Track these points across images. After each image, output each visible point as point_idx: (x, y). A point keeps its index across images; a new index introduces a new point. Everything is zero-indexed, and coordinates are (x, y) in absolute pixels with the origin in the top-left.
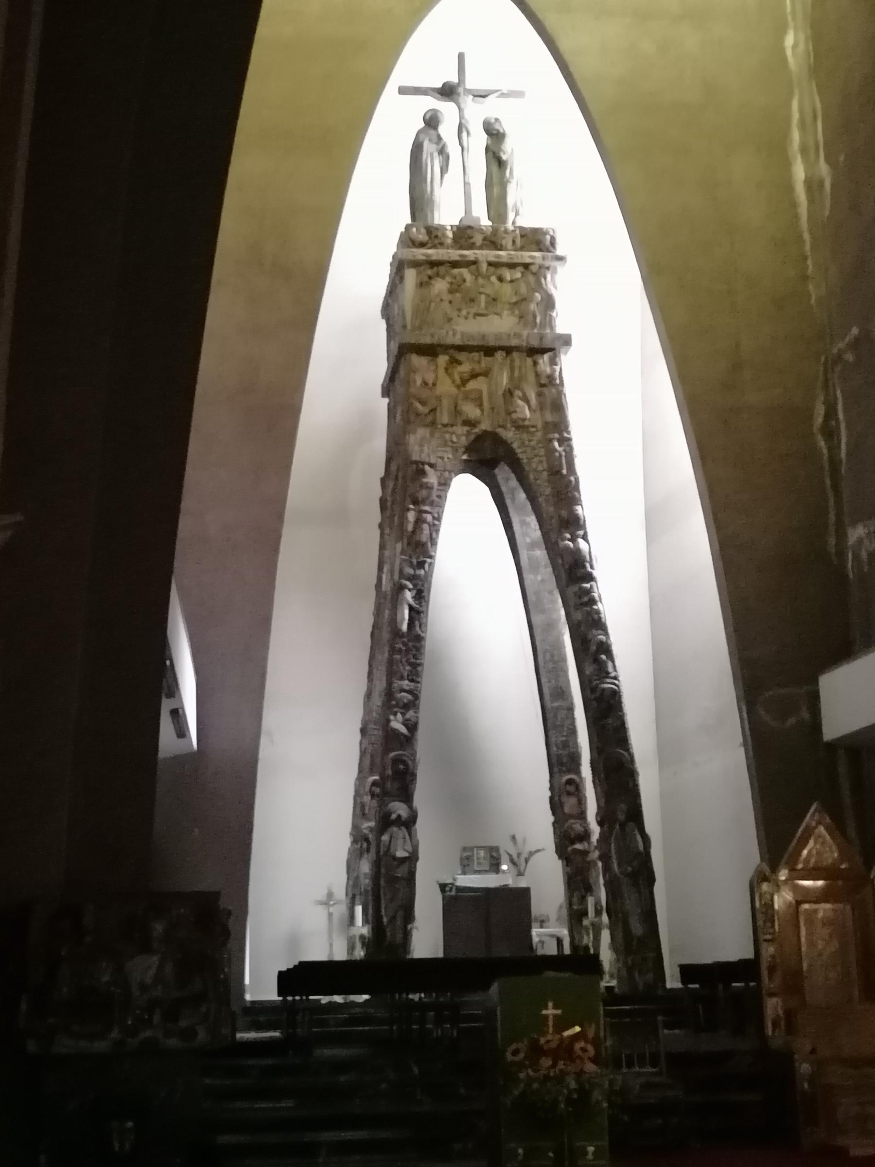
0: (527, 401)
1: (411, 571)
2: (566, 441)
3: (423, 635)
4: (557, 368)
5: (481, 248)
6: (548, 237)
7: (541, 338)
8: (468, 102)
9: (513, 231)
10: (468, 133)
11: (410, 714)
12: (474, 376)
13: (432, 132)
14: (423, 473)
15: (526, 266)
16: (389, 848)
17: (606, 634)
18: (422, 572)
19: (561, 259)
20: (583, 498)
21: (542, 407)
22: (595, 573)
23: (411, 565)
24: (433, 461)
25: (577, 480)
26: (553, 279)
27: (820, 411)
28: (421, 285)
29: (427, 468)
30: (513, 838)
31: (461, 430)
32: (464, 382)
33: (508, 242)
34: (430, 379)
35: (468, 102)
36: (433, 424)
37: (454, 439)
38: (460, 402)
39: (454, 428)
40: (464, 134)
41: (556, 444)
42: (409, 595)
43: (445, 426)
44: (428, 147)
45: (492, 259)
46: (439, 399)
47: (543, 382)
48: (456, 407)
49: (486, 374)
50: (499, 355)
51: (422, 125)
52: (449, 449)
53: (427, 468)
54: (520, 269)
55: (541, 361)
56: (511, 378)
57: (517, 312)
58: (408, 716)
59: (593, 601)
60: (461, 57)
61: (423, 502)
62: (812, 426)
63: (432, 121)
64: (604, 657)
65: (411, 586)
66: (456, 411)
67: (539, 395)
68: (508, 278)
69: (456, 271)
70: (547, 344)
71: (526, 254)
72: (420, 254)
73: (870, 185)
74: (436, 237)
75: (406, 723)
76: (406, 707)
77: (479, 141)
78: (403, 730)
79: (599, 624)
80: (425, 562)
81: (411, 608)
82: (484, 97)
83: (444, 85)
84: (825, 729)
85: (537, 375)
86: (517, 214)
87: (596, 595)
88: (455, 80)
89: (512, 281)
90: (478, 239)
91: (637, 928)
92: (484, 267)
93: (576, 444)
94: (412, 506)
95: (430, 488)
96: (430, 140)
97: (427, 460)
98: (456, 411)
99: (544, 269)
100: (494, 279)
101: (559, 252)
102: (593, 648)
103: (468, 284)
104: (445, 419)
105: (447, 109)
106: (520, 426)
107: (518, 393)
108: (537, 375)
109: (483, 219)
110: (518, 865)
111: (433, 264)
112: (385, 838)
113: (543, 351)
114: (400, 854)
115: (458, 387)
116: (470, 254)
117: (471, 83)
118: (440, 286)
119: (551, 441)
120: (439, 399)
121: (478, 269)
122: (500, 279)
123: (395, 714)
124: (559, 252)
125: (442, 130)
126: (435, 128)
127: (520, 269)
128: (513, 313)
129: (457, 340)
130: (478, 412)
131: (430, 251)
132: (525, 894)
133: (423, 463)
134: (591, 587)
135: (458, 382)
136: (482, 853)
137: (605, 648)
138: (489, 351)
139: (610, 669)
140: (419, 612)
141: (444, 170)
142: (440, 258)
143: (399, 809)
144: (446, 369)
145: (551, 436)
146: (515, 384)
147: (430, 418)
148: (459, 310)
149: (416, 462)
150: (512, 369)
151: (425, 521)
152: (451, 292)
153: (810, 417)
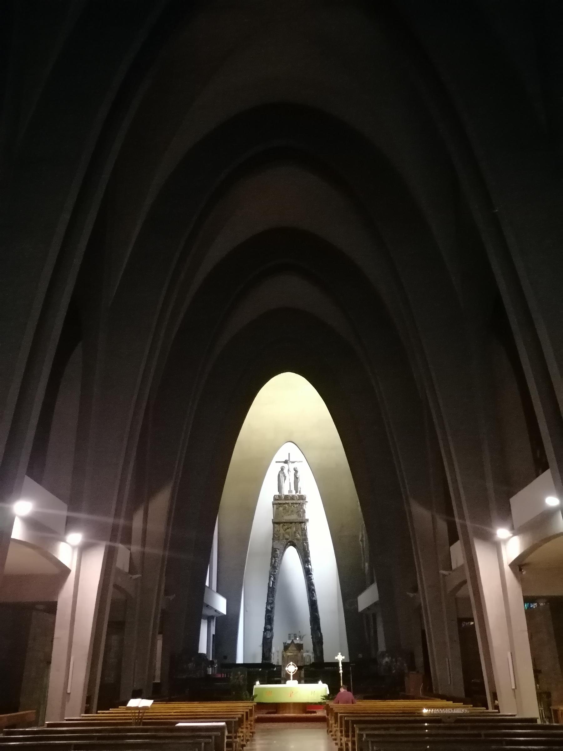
0: (299, 533)
1: (273, 573)
2: (307, 543)
3: (275, 587)
4: (306, 526)
5: (290, 500)
6: (304, 497)
7: (302, 519)
8: (290, 464)
9: (297, 496)
10: (290, 472)
11: (272, 605)
13: (282, 471)
14: (277, 551)
15: (299, 504)
16: (266, 636)
17: (314, 587)
18: (275, 573)
19: (307, 502)
20: (310, 556)
21: (302, 535)
24: (278, 548)
25: (309, 552)
27: (360, 536)
28: (277, 508)
29: (277, 549)
30: (299, 632)
31: (285, 541)
32: (286, 530)
33: (295, 499)
34: (278, 530)
35: (290, 464)
36: (279, 540)
37: (283, 543)
38: (285, 535)
39: (284, 540)
40: (289, 472)
41: (305, 544)
42: (272, 579)
43: (282, 540)
45: (292, 502)
46: (280, 534)
47: (302, 529)
48: (284, 535)
50: (293, 524)
51: (281, 470)
52: (282, 545)
53: (277, 549)
54: (298, 504)
55: (302, 525)
56: (296, 529)
57: (297, 514)
58: (271, 606)
59: (311, 579)
60: (289, 454)
61: (276, 558)
62: (359, 540)
63: (282, 469)
64: (313, 592)
65: (273, 576)
66: (284, 536)
67: (302, 532)
68: (295, 506)
69: (285, 505)
71: (300, 501)
72: (277, 502)
73: (298, 544)
74: (281, 498)
76: (271, 604)
77: (293, 472)
80: (276, 571)
81: (272, 581)
82: (294, 463)
83: (285, 460)
84: (359, 609)
85: (301, 528)
86: (300, 489)
87: (312, 578)
89: (296, 507)
90: (289, 498)
91: (319, 655)
93: (309, 543)
94: (274, 558)
95: (277, 554)
96: (282, 474)
97: (277, 548)
98: (284, 536)
99: (303, 504)
100: (292, 507)
101: (307, 500)
102: (311, 590)
103: (287, 508)
104: (281, 539)
105: (285, 465)
106: (298, 540)
107: (297, 532)
108: (301, 528)
109: (294, 493)
110: (301, 638)
111: (280, 504)
112: (265, 633)
113: (302, 522)
114: (268, 637)
115: (284, 531)
116: (287, 501)
117: (291, 460)
118: (281, 509)
119: (304, 543)
120: (280, 534)
121: (289, 505)
123: (268, 606)
124: (307, 500)
125: (284, 471)
126: (283, 471)
127: (298, 504)
128: (296, 514)
129: (284, 521)
130: (289, 536)
131: (279, 501)
132: (302, 644)
133: (276, 549)
134: (311, 576)
135: (284, 530)
136: (293, 635)
137: (314, 590)
138: (291, 523)
139: (315, 595)
140: (274, 582)
141: (285, 479)
142: (281, 503)
143: (269, 627)
144: (282, 527)
145: (304, 542)
147: (278, 539)
148: (285, 514)
149: (275, 549)
150: (296, 527)
151: (276, 562)
152: (283, 510)
153: (358, 538)
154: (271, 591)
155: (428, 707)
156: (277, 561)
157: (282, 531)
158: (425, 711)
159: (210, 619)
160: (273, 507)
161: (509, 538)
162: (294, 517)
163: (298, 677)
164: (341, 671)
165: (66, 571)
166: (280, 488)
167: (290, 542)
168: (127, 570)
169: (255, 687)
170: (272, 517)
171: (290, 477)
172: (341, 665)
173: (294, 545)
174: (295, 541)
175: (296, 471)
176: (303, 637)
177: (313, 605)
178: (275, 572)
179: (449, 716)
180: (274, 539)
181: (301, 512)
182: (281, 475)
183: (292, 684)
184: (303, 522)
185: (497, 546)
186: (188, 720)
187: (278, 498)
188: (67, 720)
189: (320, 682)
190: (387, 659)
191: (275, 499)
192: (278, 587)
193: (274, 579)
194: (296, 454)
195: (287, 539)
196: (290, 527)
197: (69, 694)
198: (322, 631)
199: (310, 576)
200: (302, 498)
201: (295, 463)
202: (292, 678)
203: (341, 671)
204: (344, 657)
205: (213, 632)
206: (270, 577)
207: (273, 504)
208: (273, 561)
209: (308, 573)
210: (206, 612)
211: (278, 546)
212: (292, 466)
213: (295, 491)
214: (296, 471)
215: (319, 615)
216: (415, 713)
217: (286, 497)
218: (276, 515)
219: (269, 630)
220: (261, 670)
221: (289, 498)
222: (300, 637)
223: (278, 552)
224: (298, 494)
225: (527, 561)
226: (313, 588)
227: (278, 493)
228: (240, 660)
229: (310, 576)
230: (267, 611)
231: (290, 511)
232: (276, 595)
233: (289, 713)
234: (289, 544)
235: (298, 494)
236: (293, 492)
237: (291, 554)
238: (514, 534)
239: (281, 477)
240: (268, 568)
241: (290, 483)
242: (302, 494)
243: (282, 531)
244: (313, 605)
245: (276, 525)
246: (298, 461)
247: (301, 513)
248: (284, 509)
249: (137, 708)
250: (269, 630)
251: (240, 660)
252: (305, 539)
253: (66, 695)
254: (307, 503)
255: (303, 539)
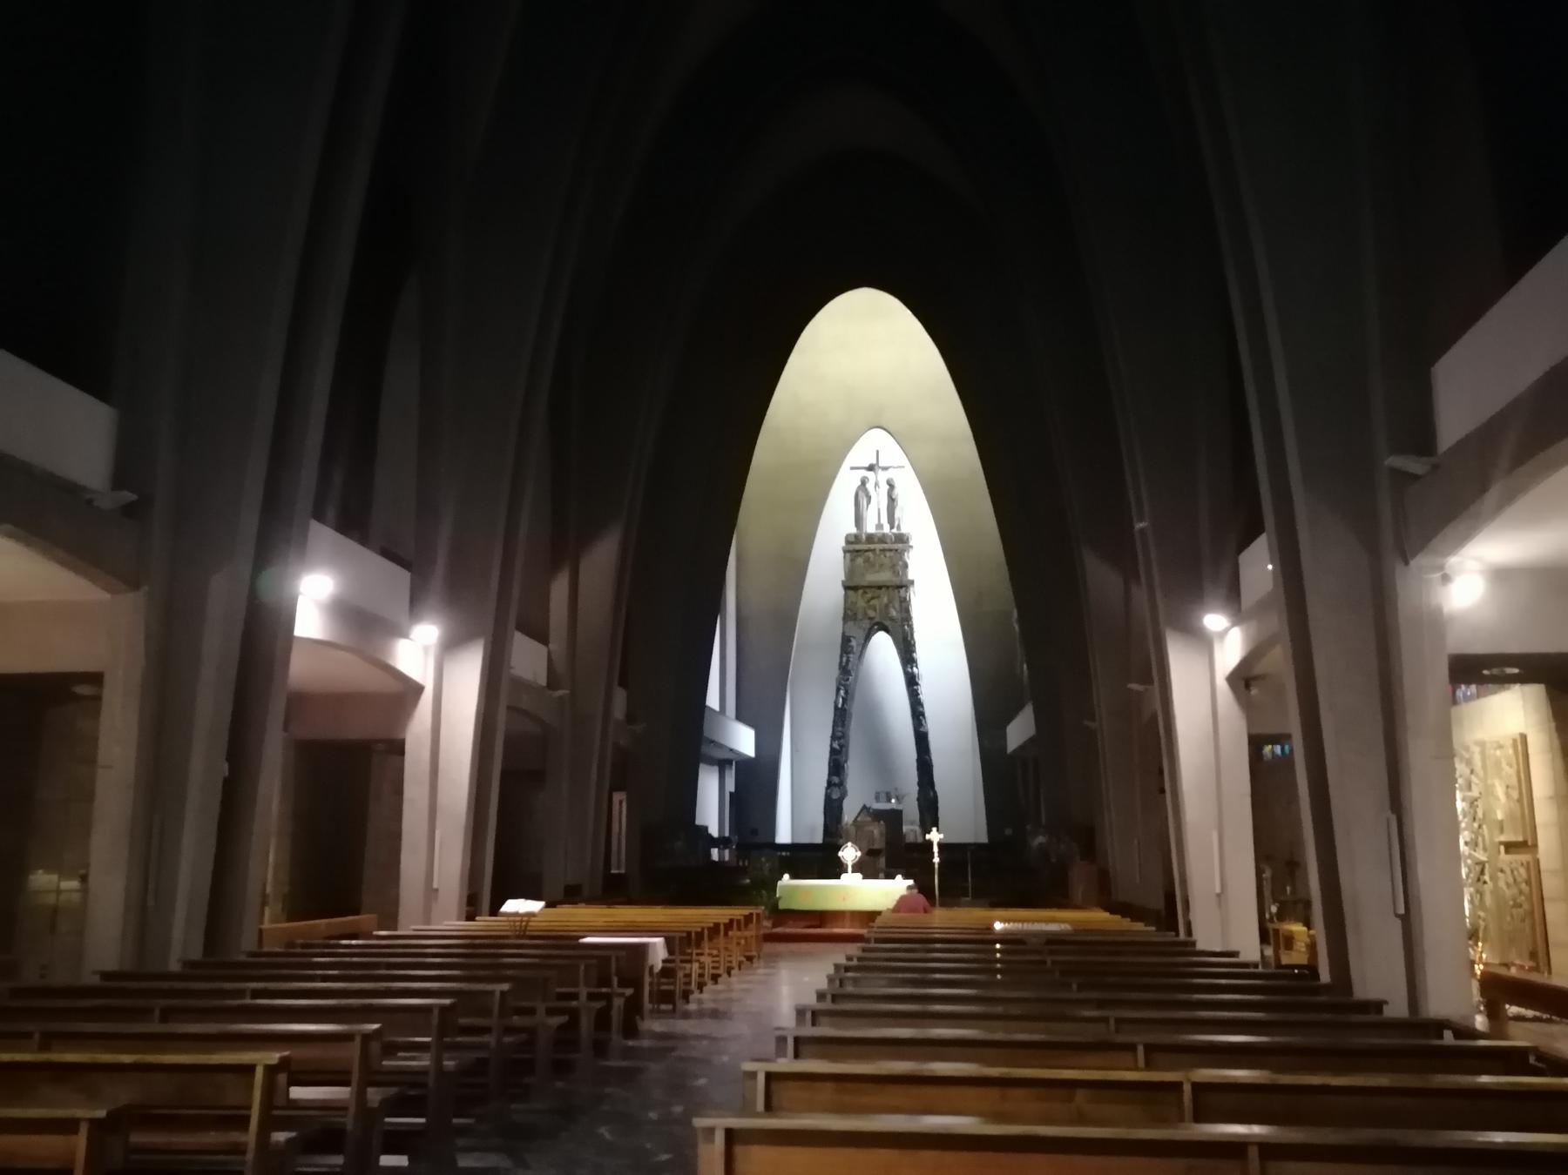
0: (895, 608)
2: (911, 627)
5: (877, 543)
7: (901, 581)
8: (880, 472)
11: (842, 741)
12: (873, 598)
14: (850, 641)
15: (896, 550)
20: (917, 650)
21: (901, 611)
22: (920, 682)
23: (843, 679)
26: (908, 557)
32: (869, 601)
33: (888, 541)
42: (842, 692)
44: (861, 494)
49: (878, 597)
50: (883, 589)
56: (888, 599)
59: (918, 694)
60: (878, 452)
61: (849, 653)
63: (864, 482)
67: (901, 606)
69: (867, 554)
70: (904, 583)
75: (839, 745)
76: (840, 738)
78: (838, 747)
79: (921, 704)
81: (843, 698)
87: (919, 692)
88: (875, 462)
90: (876, 540)
92: (878, 552)
98: (866, 614)
100: (882, 556)
105: (870, 475)
106: (892, 619)
108: (900, 597)
109: (886, 529)
111: (858, 551)
113: (901, 587)
116: (872, 546)
117: (880, 465)
118: (860, 560)
119: (904, 626)
122: (885, 556)
125: (868, 486)
129: (865, 584)
137: (923, 714)
138: (880, 588)
139: (923, 722)
141: (869, 502)
143: (836, 780)
146: (890, 601)
154: (841, 716)
155: (1003, 920)
156: (851, 659)
157: (861, 603)
158: (998, 926)
159: (723, 765)
160: (844, 557)
161: (1226, 631)
162: (884, 577)
163: (859, 867)
164: (936, 860)
165: (417, 689)
166: (859, 520)
167: (877, 624)
168: (543, 681)
169: (779, 883)
170: (843, 577)
171: (879, 499)
172: (936, 849)
173: (887, 631)
174: (887, 623)
175: (891, 486)
176: (903, 798)
177: (922, 740)
178: (848, 679)
179: (1036, 934)
180: (846, 618)
181: (899, 566)
182: (862, 495)
183: (851, 880)
184: (905, 585)
185: (1205, 643)
186: (621, 934)
187: (853, 539)
188: (415, 930)
189: (899, 877)
190: (1041, 839)
191: (848, 542)
192: (855, 709)
193: (846, 693)
194: (892, 453)
195: (871, 619)
196: (876, 595)
197: (437, 890)
198: (937, 788)
199: (915, 687)
200: (902, 539)
201: (890, 470)
202: (850, 869)
203: (936, 860)
204: (942, 836)
205: (730, 786)
206: (838, 690)
207: (845, 551)
208: (844, 659)
209: (912, 682)
210: (705, 749)
211: (857, 633)
212: (883, 477)
213: (889, 526)
214: (891, 486)
215: (931, 760)
216: (1312, 937)
217: (870, 538)
218: (850, 572)
219: (835, 785)
220: (709, 855)
221: (876, 540)
222: (898, 799)
223: (854, 643)
224: (895, 531)
225: (1259, 669)
226: (921, 709)
227: (854, 530)
228: (784, 835)
229: (915, 687)
230: (833, 752)
231: (877, 565)
232: (852, 723)
233: (843, 927)
234: (876, 627)
235: (895, 531)
236: (885, 528)
237: (882, 647)
238: (1234, 624)
239: (860, 499)
240: (835, 672)
241: (879, 510)
242: (904, 530)
243: (861, 603)
244: (922, 740)
245: (851, 593)
246: (895, 466)
247: (899, 568)
248: (867, 560)
249: (516, 914)
250: (835, 785)
251: (784, 835)
252: (907, 618)
253: (431, 893)
254: (910, 550)
255: (902, 618)
